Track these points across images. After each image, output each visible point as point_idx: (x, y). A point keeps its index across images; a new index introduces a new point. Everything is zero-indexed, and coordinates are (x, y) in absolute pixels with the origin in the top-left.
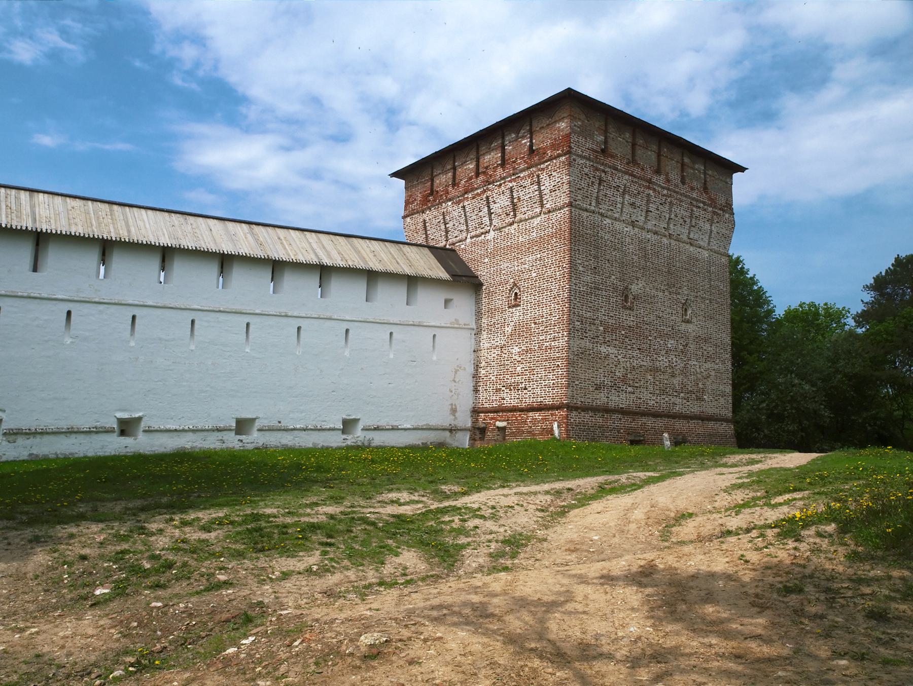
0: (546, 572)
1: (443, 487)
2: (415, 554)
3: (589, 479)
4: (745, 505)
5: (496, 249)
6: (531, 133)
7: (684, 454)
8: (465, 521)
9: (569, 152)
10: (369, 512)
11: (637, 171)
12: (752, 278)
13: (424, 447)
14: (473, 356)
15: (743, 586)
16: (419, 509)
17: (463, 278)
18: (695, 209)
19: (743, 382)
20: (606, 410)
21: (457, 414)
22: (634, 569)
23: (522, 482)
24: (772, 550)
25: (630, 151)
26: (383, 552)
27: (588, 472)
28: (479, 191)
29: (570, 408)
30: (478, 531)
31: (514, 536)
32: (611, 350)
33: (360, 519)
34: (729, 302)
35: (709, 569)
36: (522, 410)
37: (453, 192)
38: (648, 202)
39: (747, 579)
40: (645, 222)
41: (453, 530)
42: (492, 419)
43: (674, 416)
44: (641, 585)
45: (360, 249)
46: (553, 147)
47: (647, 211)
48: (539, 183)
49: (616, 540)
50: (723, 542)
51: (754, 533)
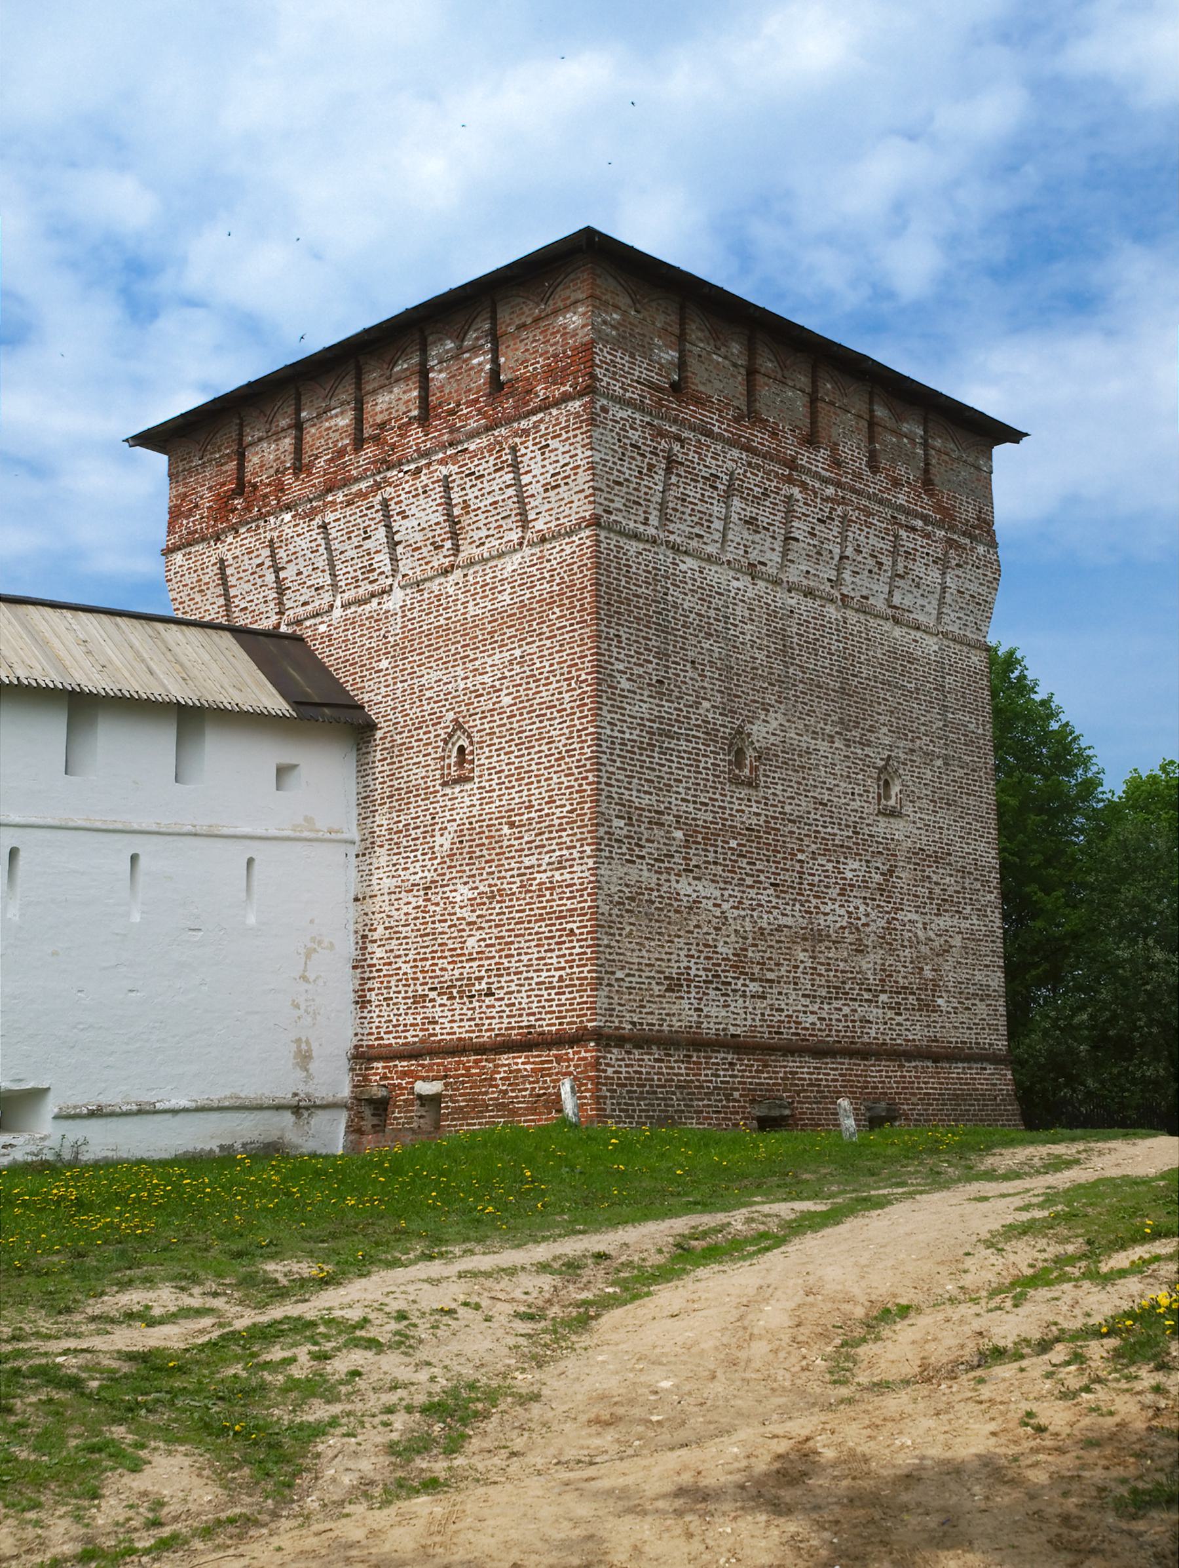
0: (535, 1485)
1: (270, 1267)
2: (187, 1462)
3: (651, 1227)
4: (1039, 1279)
5: (408, 635)
6: (495, 339)
7: (890, 1151)
8: (323, 1357)
9: (590, 390)
10: (60, 1352)
11: (760, 439)
12: (1044, 703)
13: (225, 1159)
14: (352, 912)
15: (1032, 1497)
16: (202, 1332)
17: (324, 710)
18: (902, 533)
19: (1031, 961)
20: (696, 1043)
21: (312, 1067)
22: (761, 1466)
23: (479, 1241)
24: (1101, 1394)
25: (742, 389)
26: (98, 1463)
27: (648, 1206)
28: (363, 485)
29: (605, 1039)
30: (360, 1383)
31: (454, 1393)
32: (706, 889)
33: (36, 1372)
34: (991, 761)
35: (949, 1455)
36: (481, 1050)
37: (295, 488)
38: (789, 514)
39: (1039, 1477)
40: (782, 567)
41: (293, 1385)
42: (405, 1074)
43: (865, 1053)
44: (779, 1508)
45: (48, 634)
46: (552, 375)
47: (788, 539)
48: (515, 466)
49: (718, 1387)
50: (981, 1381)
51: (1059, 1353)
